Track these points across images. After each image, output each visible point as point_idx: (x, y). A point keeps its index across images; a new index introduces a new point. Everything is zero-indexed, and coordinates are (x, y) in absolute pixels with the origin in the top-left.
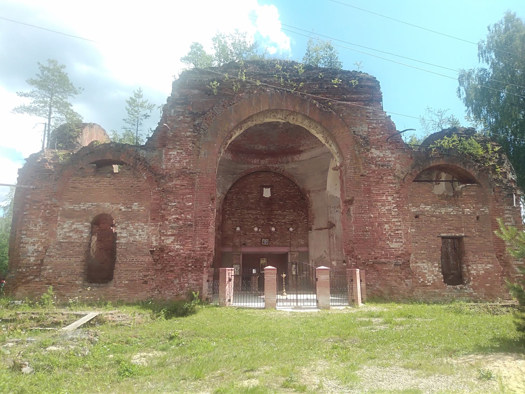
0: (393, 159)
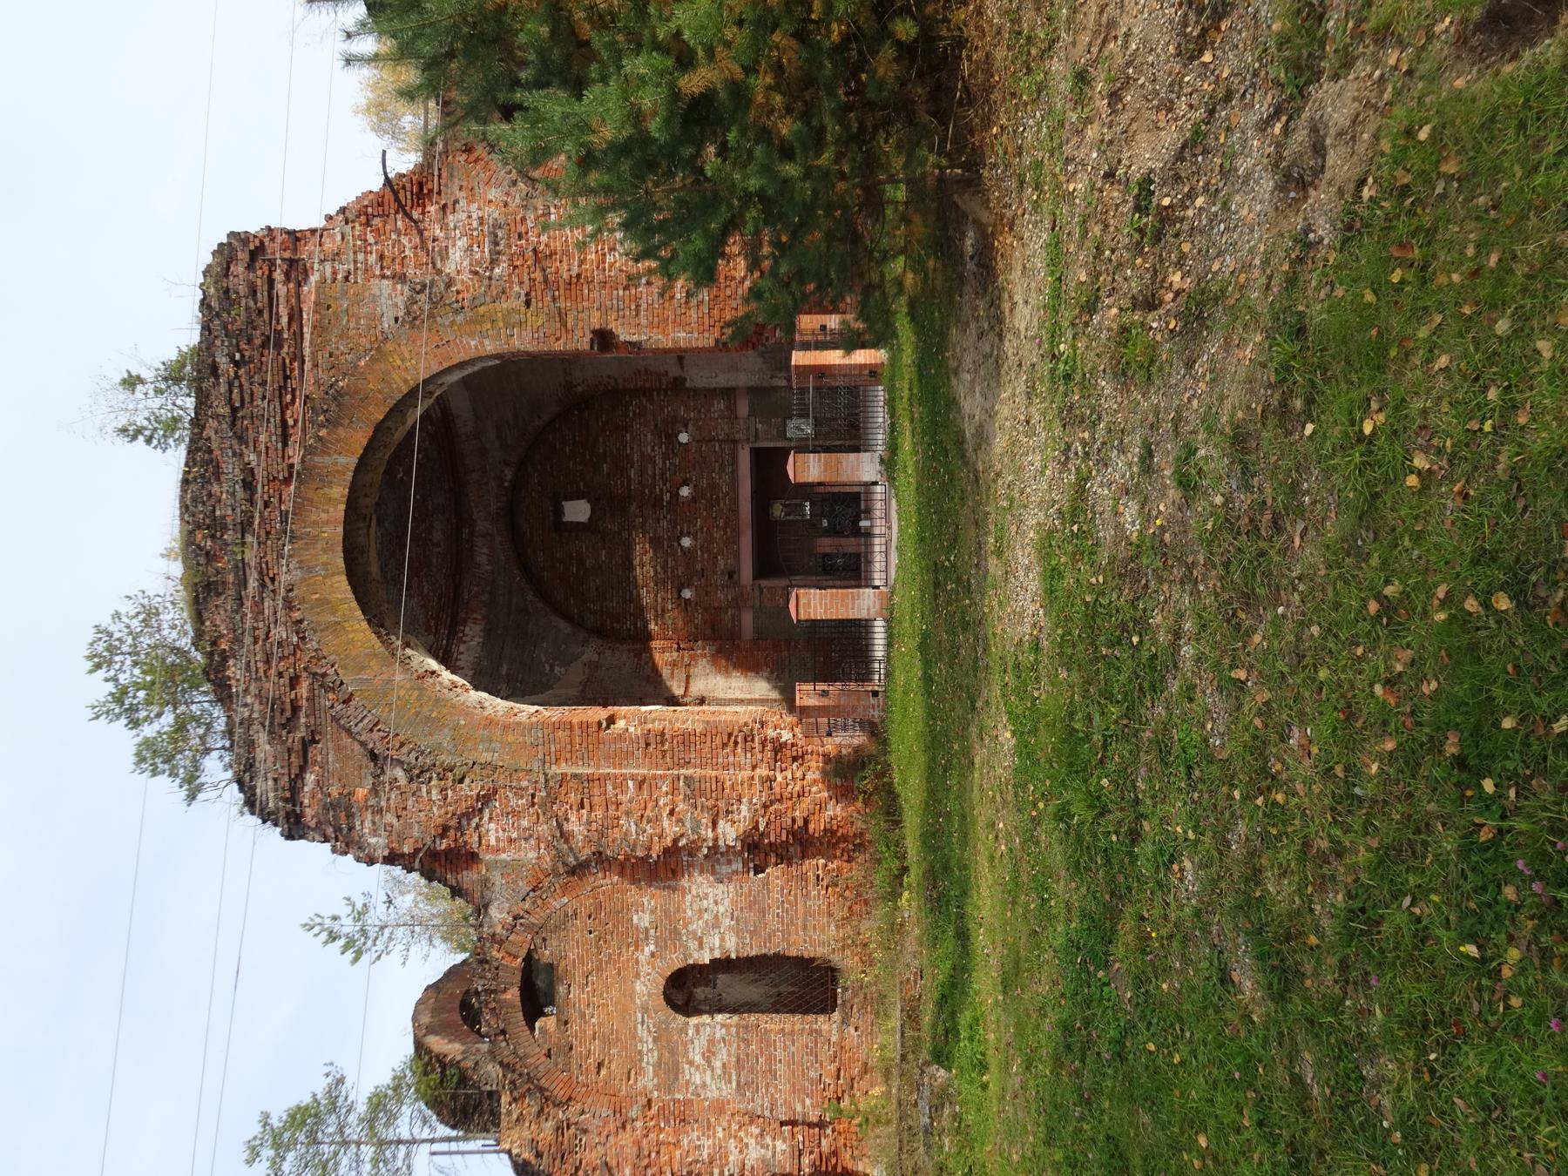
0: (474, 207)
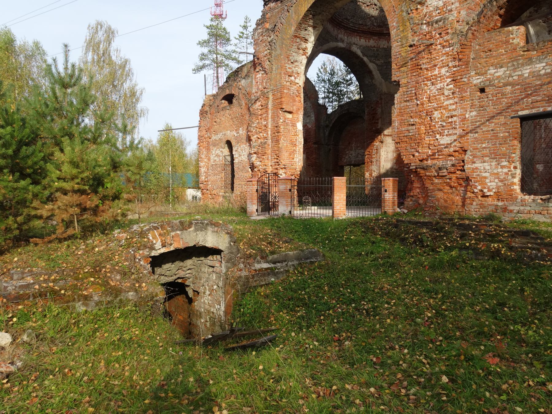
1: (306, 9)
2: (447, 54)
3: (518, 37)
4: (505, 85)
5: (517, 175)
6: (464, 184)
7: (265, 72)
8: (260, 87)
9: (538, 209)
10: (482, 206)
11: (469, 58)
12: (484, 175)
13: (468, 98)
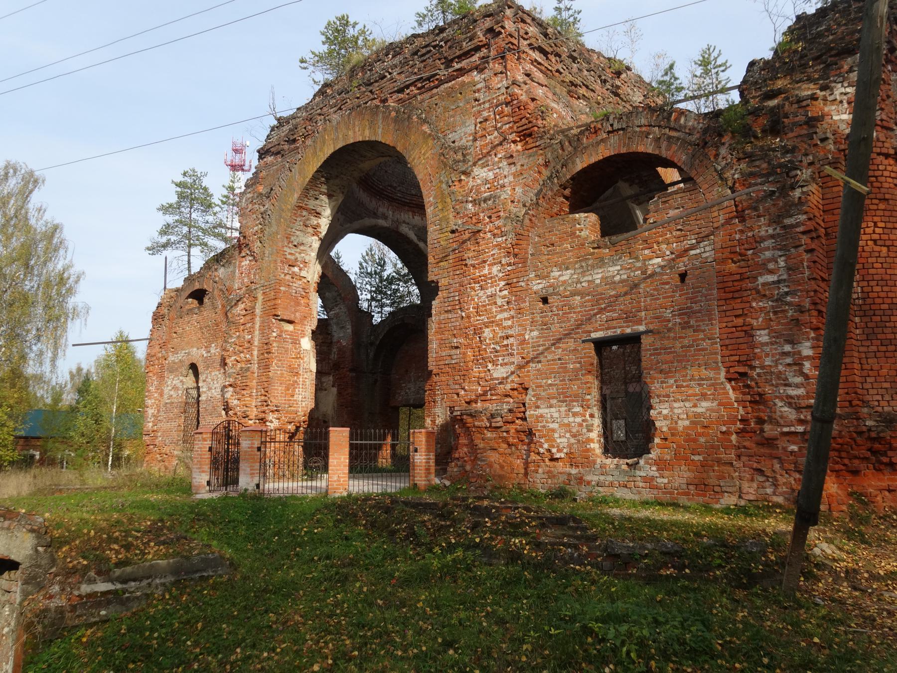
0: (511, 178)
1: (315, 169)
2: (498, 245)
3: (587, 228)
4: (573, 294)
5: (595, 427)
6: (527, 441)
7: (254, 258)
8: (246, 280)
9: (624, 479)
10: (550, 475)
11: (526, 253)
12: (552, 426)
13: (527, 310)
